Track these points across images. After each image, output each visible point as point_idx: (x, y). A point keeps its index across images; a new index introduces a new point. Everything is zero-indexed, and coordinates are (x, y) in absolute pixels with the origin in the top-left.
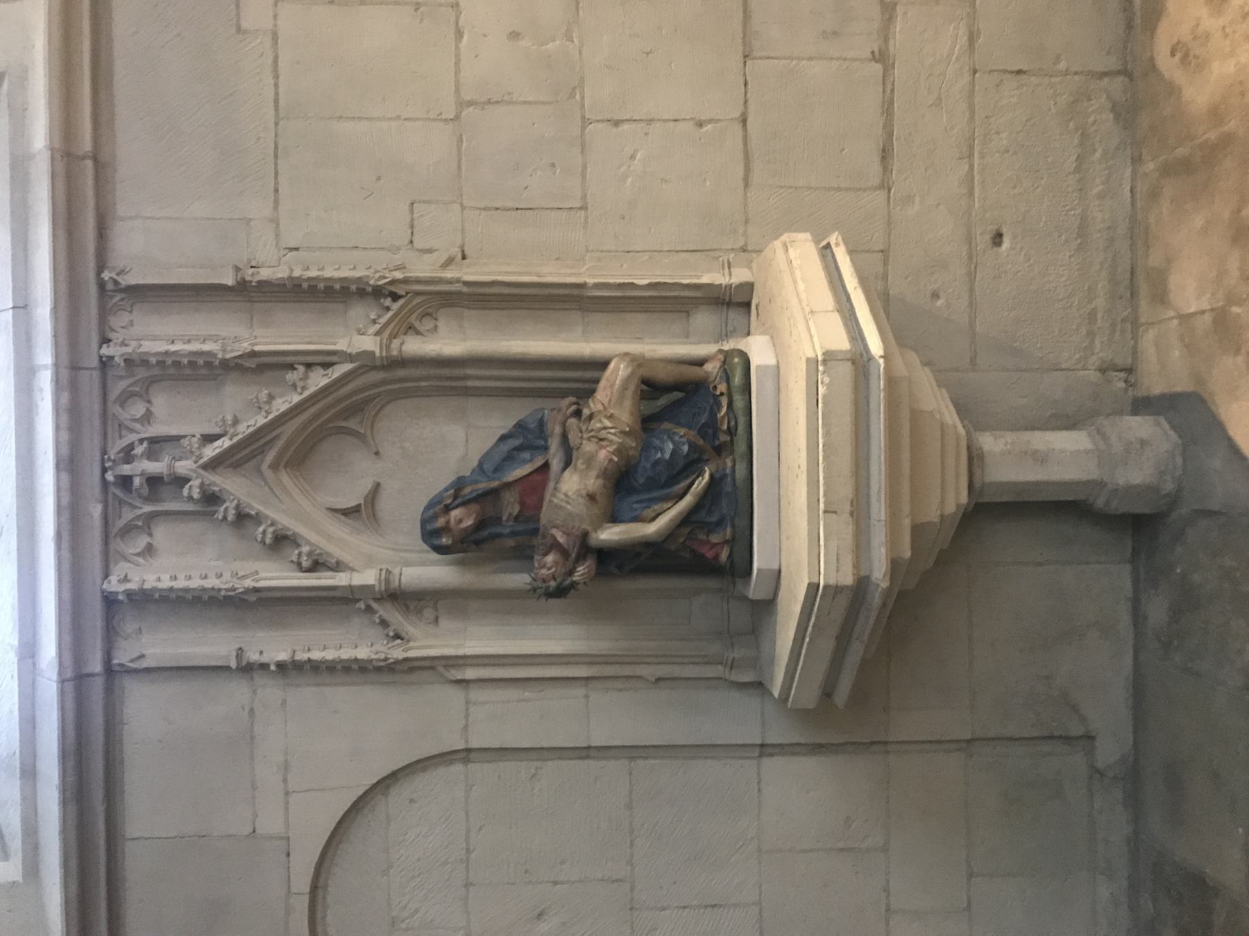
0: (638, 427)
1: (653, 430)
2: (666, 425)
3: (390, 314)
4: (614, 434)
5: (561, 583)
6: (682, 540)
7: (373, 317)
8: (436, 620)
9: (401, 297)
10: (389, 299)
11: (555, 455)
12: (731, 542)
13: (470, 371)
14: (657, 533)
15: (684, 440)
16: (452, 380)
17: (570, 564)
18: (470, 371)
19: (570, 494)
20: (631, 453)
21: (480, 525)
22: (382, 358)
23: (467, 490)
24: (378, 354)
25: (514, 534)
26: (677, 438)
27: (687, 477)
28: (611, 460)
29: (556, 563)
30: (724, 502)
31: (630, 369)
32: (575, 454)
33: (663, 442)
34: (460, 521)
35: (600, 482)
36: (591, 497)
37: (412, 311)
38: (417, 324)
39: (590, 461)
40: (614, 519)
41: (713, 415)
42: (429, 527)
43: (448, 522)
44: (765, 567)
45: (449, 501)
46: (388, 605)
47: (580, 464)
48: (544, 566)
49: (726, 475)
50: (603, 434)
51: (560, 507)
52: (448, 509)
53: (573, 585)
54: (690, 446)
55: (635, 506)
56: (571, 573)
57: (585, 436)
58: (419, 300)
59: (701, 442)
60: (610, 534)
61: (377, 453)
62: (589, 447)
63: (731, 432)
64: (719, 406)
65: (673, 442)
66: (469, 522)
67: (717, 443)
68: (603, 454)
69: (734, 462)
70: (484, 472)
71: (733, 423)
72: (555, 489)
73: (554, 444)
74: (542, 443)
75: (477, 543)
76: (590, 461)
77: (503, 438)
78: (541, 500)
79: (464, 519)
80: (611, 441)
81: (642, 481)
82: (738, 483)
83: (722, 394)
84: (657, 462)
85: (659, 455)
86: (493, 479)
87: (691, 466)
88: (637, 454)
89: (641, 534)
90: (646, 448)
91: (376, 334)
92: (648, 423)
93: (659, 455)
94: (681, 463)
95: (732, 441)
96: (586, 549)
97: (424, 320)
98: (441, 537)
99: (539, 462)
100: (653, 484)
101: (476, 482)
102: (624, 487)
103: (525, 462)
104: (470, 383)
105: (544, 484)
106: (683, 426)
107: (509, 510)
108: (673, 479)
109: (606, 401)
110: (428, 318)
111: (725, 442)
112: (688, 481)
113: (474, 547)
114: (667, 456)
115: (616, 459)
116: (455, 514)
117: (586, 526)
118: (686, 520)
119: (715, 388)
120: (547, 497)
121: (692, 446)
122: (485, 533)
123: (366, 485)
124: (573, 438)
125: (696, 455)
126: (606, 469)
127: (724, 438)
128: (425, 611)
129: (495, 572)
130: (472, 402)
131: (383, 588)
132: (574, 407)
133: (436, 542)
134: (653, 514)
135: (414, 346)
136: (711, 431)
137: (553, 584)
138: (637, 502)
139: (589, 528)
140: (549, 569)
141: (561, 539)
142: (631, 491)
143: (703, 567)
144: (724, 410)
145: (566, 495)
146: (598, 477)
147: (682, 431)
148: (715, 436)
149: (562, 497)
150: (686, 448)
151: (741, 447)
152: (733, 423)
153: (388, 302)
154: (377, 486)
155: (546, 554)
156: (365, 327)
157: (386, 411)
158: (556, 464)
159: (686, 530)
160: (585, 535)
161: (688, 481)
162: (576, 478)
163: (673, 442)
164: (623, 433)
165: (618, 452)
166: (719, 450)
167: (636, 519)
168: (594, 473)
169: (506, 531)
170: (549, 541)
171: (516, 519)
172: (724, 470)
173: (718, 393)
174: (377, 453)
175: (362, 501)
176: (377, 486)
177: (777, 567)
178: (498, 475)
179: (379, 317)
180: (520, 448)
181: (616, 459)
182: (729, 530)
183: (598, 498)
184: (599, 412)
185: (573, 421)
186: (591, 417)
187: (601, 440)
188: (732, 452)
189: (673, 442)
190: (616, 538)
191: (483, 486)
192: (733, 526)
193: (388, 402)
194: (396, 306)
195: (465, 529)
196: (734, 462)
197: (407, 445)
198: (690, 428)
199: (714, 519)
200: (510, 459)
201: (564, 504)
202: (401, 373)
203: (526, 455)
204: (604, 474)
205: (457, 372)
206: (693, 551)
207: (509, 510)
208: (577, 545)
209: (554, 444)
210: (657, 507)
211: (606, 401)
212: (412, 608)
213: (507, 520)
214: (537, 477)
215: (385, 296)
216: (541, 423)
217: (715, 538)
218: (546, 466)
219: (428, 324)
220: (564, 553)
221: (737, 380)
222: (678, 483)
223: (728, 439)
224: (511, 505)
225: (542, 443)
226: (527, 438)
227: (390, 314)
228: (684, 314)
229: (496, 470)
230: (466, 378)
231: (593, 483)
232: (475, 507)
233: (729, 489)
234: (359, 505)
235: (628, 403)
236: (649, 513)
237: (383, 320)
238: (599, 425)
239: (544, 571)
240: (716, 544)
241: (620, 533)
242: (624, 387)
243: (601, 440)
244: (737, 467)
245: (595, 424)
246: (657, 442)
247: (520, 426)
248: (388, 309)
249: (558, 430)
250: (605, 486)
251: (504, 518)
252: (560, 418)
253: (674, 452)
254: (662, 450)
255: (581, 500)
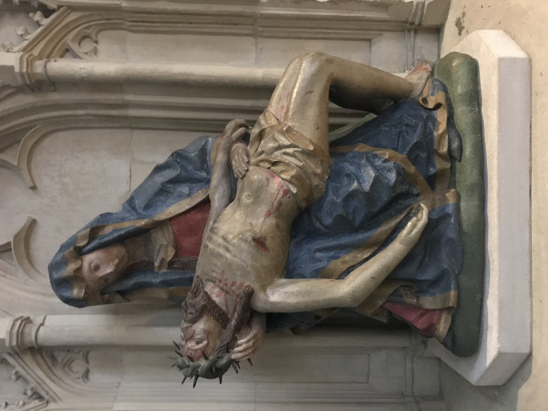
0: (325, 148)
1: (344, 154)
2: (361, 148)
3: (41, 28)
4: (293, 155)
5: (215, 362)
6: (380, 303)
7: (20, 33)
8: (86, 375)
9: (54, 11)
10: (39, 13)
11: (216, 187)
12: (454, 311)
13: (130, 97)
14: (353, 295)
15: (390, 164)
16: (108, 107)
17: (227, 334)
18: (130, 97)
19: (230, 237)
20: (316, 182)
21: (125, 272)
22: (22, 74)
23: (108, 230)
24: (17, 70)
25: (166, 284)
26: (378, 163)
27: (399, 212)
28: (287, 192)
29: (208, 333)
30: (444, 254)
31: (316, 65)
32: (240, 184)
33: (359, 167)
34: (97, 268)
35: (272, 221)
36: (259, 242)
37: (68, 28)
38: (74, 47)
39: (258, 193)
40: (289, 271)
41: (427, 134)
42: (56, 276)
43: (79, 270)
44: (509, 349)
45: (81, 244)
46: (28, 358)
47: (245, 197)
48: (191, 338)
49: (448, 216)
50: (278, 155)
51: (219, 256)
52: (80, 253)
53: (232, 362)
54: (398, 174)
55: (318, 255)
56: (229, 347)
57: (253, 161)
58: (73, 16)
59: (412, 169)
60: (284, 294)
61: (34, 188)
62: (257, 175)
63: (453, 157)
64: (435, 122)
65: (371, 170)
66: (108, 270)
67: (432, 171)
68: (276, 184)
69: (458, 197)
70: (134, 208)
71: (455, 145)
72: (212, 230)
73: (217, 176)
74: (204, 174)
75: (123, 293)
76: (258, 193)
77: (159, 169)
78: (199, 244)
79: (100, 264)
80: (288, 165)
81: (328, 221)
82: (466, 226)
83: (438, 106)
84: (352, 195)
85: (355, 185)
86: (144, 217)
87: (392, 204)
88: (322, 185)
89: (328, 296)
90: (335, 175)
91: (24, 50)
92: (337, 147)
93: (355, 185)
94: (385, 197)
95: (452, 168)
96: (250, 313)
97: (83, 43)
98: (72, 288)
99: (198, 198)
100: (344, 225)
101: (123, 219)
102: (303, 229)
103: (181, 197)
104: (132, 112)
105: (205, 221)
106: (385, 147)
107: (161, 255)
108: (372, 220)
109: (281, 115)
110: (87, 40)
111: (444, 170)
112: (393, 223)
113: (118, 297)
114: (367, 187)
115: (294, 190)
116: (90, 259)
117: (251, 282)
118: (393, 277)
119: (425, 100)
120: (205, 241)
121: (401, 174)
122: (131, 282)
123: (20, 223)
124: (238, 165)
125: (404, 188)
126: (280, 204)
127: (440, 164)
128: (74, 364)
129: (148, 325)
130: (138, 135)
131: (14, 343)
132: (241, 130)
133: (66, 294)
134: (345, 267)
135: (62, 66)
136: (424, 155)
137: (203, 363)
138: (320, 250)
139: (256, 286)
140: (198, 343)
141: (217, 297)
142: (313, 234)
143: (397, 326)
144: (442, 127)
145: (225, 239)
146: (269, 214)
147: (387, 154)
148: (429, 161)
149: (220, 241)
150: (392, 177)
151: (466, 173)
152: (455, 145)
153: (38, 16)
154: (33, 223)
155: (194, 321)
156: (12, 44)
157: (47, 142)
158: (217, 201)
159: (390, 290)
160: (250, 295)
161: (393, 223)
162: (239, 215)
163: (371, 170)
164: (305, 153)
165: (297, 180)
166: (432, 181)
167: (320, 274)
168: (263, 209)
169: (157, 280)
170: (200, 301)
171: (171, 264)
172: (444, 208)
173: (431, 105)
174: (34, 188)
175: (12, 240)
176: (33, 223)
177: (526, 351)
178: (149, 212)
179: (27, 33)
180: (176, 181)
181: (294, 190)
182: (453, 294)
183: (268, 243)
184: (272, 127)
185: (239, 147)
186: (261, 136)
187: (274, 164)
188: (453, 184)
189: (374, 167)
190: (292, 300)
191: (129, 225)
192: (458, 288)
193: (44, 136)
194: (46, 22)
195: (105, 278)
196: (458, 197)
197: (67, 180)
198: (396, 149)
199: (429, 275)
200: (164, 192)
201: (221, 251)
202: (54, 97)
203: (184, 189)
204: (277, 210)
205: (112, 97)
206: (390, 313)
207: (161, 255)
208: (239, 308)
209: (217, 176)
210: (349, 258)
211: (281, 115)
212: (59, 359)
213: (160, 267)
214: (198, 216)
215: (35, 11)
216: (203, 152)
217: (429, 302)
218: (206, 203)
219: (87, 46)
220: (221, 318)
221: (460, 89)
222: (378, 225)
223: (448, 165)
224: (163, 248)
225: (204, 174)
226: (186, 171)
227: (41, 28)
228: (367, 43)
229: (147, 207)
230: (125, 105)
231: (262, 222)
232: (117, 251)
233: (451, 234)
234: (9, 243)
235: (312, 112)
236: (338, 265)
237: (31, 37)
238: (271, 145)
239: (191, 345)
240: (427, 311)
241: (298, 294)
242: (307, 92)
243: (274, 164)
244: (463, 204)
245: (268, 144)
246: (350, 168)
247: (178, 156)
248: (38, 24)
249: (221, 157)
250: (277, 226)
251: (157, 264)
252: (223, 142)
253: (377, 181)
254: (358, 178)
255: (244, 246)
